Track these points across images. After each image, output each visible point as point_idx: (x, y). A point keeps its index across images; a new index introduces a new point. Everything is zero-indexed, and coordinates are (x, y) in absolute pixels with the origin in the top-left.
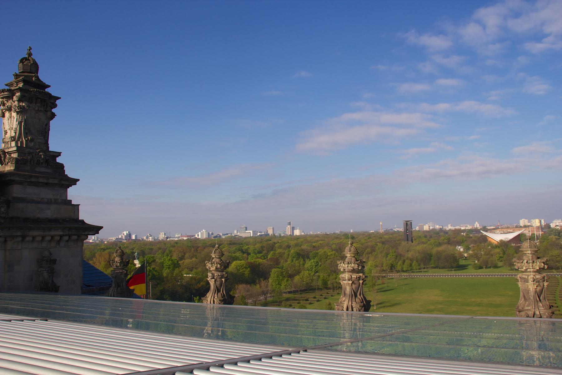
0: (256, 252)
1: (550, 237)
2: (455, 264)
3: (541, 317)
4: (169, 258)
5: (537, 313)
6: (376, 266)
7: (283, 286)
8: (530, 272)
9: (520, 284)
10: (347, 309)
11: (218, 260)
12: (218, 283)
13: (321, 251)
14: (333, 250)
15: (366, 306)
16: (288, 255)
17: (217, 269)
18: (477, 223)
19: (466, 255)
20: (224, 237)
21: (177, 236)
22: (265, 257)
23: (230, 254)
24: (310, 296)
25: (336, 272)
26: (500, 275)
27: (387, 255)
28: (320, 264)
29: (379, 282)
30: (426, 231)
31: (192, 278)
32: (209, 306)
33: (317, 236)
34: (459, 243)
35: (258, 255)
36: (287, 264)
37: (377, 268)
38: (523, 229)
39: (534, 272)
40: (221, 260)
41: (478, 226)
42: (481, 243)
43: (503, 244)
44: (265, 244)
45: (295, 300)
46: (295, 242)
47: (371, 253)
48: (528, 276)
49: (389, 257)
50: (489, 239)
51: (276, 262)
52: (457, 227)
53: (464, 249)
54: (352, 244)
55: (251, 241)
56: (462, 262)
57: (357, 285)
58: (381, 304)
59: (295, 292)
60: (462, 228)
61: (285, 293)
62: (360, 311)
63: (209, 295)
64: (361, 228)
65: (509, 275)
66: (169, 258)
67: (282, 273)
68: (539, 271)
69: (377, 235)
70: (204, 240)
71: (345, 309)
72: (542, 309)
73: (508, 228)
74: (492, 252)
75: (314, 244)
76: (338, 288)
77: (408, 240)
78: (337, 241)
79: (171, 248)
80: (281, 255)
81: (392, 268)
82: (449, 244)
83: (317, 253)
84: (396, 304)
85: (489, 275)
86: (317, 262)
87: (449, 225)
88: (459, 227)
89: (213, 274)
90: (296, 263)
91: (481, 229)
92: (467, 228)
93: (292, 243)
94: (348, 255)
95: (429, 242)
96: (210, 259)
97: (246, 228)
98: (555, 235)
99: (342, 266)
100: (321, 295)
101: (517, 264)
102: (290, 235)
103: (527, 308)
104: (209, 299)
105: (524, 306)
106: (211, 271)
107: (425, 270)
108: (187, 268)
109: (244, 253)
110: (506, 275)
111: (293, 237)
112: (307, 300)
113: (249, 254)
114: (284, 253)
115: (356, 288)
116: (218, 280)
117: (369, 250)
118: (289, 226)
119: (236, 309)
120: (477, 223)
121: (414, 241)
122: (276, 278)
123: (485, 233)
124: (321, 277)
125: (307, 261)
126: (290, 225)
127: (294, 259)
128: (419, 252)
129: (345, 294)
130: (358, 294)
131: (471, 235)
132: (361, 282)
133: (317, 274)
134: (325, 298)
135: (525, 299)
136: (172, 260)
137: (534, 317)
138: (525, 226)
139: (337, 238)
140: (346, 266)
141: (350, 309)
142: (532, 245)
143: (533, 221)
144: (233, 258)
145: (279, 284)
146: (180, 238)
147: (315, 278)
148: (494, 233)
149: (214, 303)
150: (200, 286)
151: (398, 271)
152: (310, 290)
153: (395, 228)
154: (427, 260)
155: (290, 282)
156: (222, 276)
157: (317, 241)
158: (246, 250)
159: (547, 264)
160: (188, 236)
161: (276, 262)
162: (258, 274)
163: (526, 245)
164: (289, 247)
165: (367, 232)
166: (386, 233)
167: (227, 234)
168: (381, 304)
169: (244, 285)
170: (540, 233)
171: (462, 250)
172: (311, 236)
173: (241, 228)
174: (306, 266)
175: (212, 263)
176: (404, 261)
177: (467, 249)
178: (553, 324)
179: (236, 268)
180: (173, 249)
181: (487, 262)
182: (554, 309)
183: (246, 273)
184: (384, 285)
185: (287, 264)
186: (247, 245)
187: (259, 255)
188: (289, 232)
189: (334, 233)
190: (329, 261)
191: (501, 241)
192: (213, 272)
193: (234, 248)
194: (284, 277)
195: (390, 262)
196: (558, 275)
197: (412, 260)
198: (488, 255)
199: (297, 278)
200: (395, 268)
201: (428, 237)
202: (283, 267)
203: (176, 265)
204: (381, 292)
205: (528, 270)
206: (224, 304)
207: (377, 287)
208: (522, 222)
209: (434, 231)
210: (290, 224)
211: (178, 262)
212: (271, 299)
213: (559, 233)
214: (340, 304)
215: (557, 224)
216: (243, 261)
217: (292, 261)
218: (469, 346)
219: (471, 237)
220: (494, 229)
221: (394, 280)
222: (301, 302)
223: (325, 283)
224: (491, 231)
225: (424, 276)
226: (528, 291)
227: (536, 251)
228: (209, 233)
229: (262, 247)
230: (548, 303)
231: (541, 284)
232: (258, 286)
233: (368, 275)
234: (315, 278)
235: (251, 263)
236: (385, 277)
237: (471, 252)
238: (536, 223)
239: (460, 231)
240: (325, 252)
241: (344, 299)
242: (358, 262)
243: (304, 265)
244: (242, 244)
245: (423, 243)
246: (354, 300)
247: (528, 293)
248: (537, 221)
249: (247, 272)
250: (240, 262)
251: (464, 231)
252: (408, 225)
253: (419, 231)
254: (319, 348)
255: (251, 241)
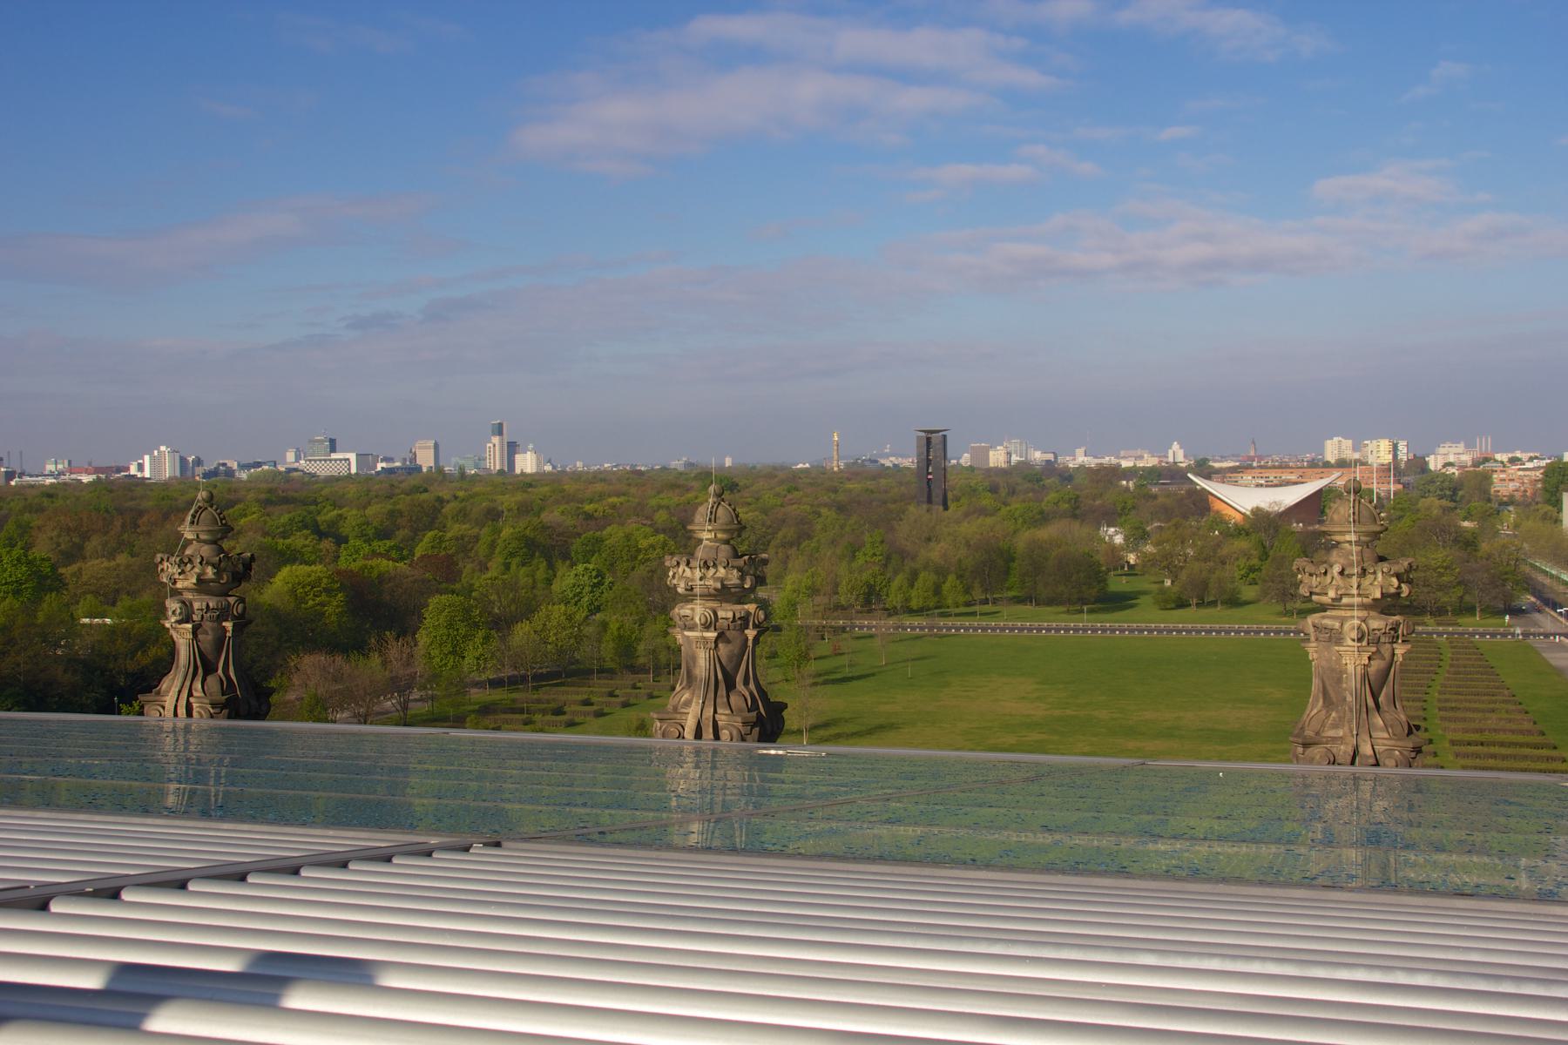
0: (371, 532)
1: (1422, 503)
2: (1092, 588)
3: (1377, 764)
4: (17, 552)
5: (1366, 749)
6: (813, 591)
7: (469, 660)
8: (1350, 606)
9: (1312, 649)
10: (698, 734)
11: (206, 550)
12: (207, 639)
13: (614, 534)
14: (657, 531)
15: (768, 723)
16: (493, 545)
17: (202, 585)
18: (1176, 446)
19: (1132, 558)
20: (244, 476)
21: (50, 467)
22: (402, 552)
23: (268, 540)
24: (570, 696)
25: (663, 601)
26: (1247, 632)
27: (854, 551)
28: (609, 579)
29: (824, 648)
30: (998, 471)
31: (112, 630)
32: (168, 725)
33: (599, 477)
34: (1111, 516)
35: (375, 543)
36: (484, 579)
37: (818, 599)
38: (1336, 474)
39: (1363, 607)
40: (221, 550)
41: (1180, 457)
42: (1185, 517)
43: (1263, 521)
44: (403, 502)
45: (513, 711)
46: (519, 497)
47: (795, 543)
48: (1343, 620)
49: (861, 560)
50: (1217, 506)
51: (446, 570)
52: (1107, 460)
53: (1126, 539)
54: (719, 495)
55: (352, 491)
56: (1117, 584)
57: (735, 647)
58: (826, 725)
59: (513, 682)
60: (1125, 464)
61: (477, 684)
62: (743, 740)
63: (171, 687)
64: (763, 456)
65: (1277, 632)
66: (17, 552)
67: (467, 611)
68: (1387, 604)
69: (819, 479)
70: (165, 485)
71: (689, 733)
72: (1382, 737)
73: (1283, 466)
74: (1224, 551)
75: (588, 508)
76: (670, 665)
77: (930, 501)
78: (672, 499)
79: (27, 516)
80: (466, 545)
81: (871, 598)
82: (1075, 517)
83: (600, 541)
84: (881, 728)
85: (1209, 632)
86: (600, 574)
87: (1080, 452)
88: (1114, 461)
89: (187, 606)
90: (522, 575)
91: (1189, 469)
92: (1140, 464)
93: (507, 501)
94: (705, 536)
95: (1004, 510)
96: (174, 546)
97: (333, 442)
98: (1441, 497)
99: (682, 575)
100: (611, 694)
101: (1306, 578)
102: (501, 472)
103: (1331, 733)
104: (169, 701)
105: (1323, 725)
106: (176, 593)
107: (988, 608)
108: (96, 593)
109: (321, 535)
110: (1267, 632)
111: (508, 480)
112: (559, 712)
113: (341, 540)
114: (477, 538)
115: (730, 658)
116: (207, 625)
117: (788, 532)
118: (496, 440)
119: (269, 732)
120: (1176, 446)
121: (952, 506)
122: (443, 631)
123: (1202, 483)
124: (614, 626)
125: (562, 568)
126: (500, 433)
127: (515, 561)
128: (968, 545)
129: (690, 677)
130: (739, 678)
131: (1155, 490)
132: (751, 633)
133: (598, 616)
134: (626, 705)
135: (1328, 703)
136: (29, 563)
137: (1353, 763)
138: (1342, 464)
139: (673, 486)
140: (698, 574)
141: (708, 733)
142: (1365, 513)
143: (1371, 445)
144: (282, 553)
145: (454, 653)
146: (67, 478)
147: (589, 630)
148: (1235, 483)
149: (189, 713)
150: (146, 661)
151: (891, 612)
152: (570, 674)
153: (887, 456)
154: (997, 575)
155: (495, 644)
156: (224, 614)
157: (602, 496)
158: (333, 524)
159: (1409, 582)
160: (97, 470)
161: (446, 570)
162: (375, 614)
163: (1340, 513)
164: (493, 515)
165: (783, 468)
166: (855, 472)
167: (259, 465)
168: (826, 725)
169: (322, 658)
170: (1392, 488)
171: (1119, 539)
172: (577, 476)
173: (313, 442)
174: (556, 587)
175: (182, 563)
176: (913, 577)
177: (1138, 536)
178: (1419, 787)
179: (293, 592)
180: (37, 521)
181: (1204, 585)
182: (1421, 736)
183: (329, 609)
184: (844, 660)
185: (484, 579)
186: (335, 506)
187: (381, 546)
188: (494, 463)
189: (664, 469)
190: (641, 571)
191: (1257, 511)
192: (188, 596)
193: (283, 517)
194: (476, 625)
195: (865, 576)
196: (1440, 634)
197: (942, 572)
198: (1206, 560)
199: (522, 632)
200: (879, 600)
201: (1003, 492)
202: (471, 588)
203: (46, 581)
204: (826, 683)
205: (1345, 600)
206: (229, 717)
207: (813, 667)
208: (1333, 449)
209: (1024, 466)
210: (499, 430)
211: (54, 568)
212: (424, 708)
213: (1455, 490)
214: (673, 717)
215: (1452, 459)
216: (319, 567)
217: (507, 567)
218: (1123, 833)
219: (1155, 497)
220: (1233, 470)
221: (877, 642)
222: (538, 717)
223: (626, 649)
224: (1223, 475)
225: (984, 629)
226: (1338, 675)
227: (1376, 535)
228: (183, 461)
229: (392, 514)
230: (1403, 717)
231: (1386, 650)
232: (375, 660)
233: (784, 623)
234: (589, 630)
235: (349, 574)
236: (843, 629)
237: (1149, 548)
238: (1380, 452)
239: (1115, 473)
240: (628, 537)
241: (687, 696)
242: (740, 562)
243: (549, 582)
244: (315, 503)
245: (983, 512)
246: (722, 700)
247: (1339, 680)
248: (1385, 445)
249: (334, 607)
250: (307, 568)
251: (1130, 473)
252: (932, 444)
253: (971, 469)
254: (551, 838)
255: (352, 491)
